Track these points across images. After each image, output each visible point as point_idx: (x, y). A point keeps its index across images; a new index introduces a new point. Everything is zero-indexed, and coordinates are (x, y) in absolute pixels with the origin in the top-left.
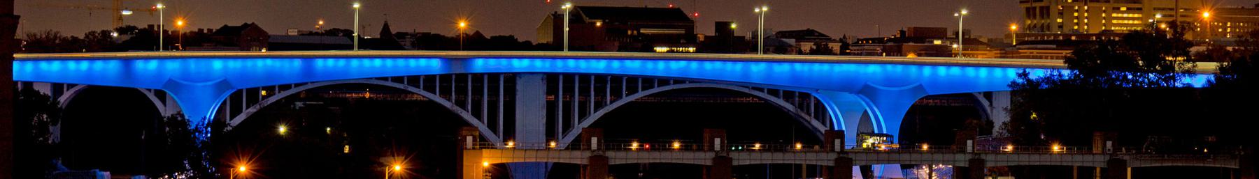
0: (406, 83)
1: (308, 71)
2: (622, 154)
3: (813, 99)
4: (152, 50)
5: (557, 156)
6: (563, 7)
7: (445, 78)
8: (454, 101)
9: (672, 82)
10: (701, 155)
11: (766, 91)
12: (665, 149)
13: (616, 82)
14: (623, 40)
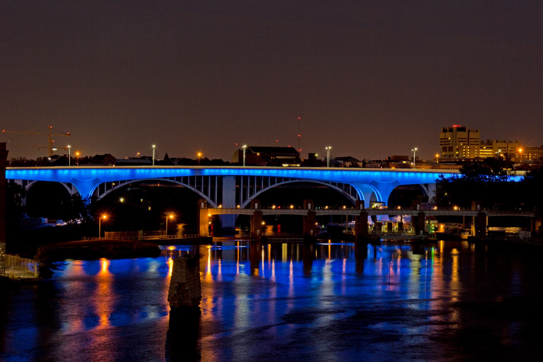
2: (268, 211)
6: (243, 147)
7: (192, 178)
9: (290, 179)
12: (287, 209)
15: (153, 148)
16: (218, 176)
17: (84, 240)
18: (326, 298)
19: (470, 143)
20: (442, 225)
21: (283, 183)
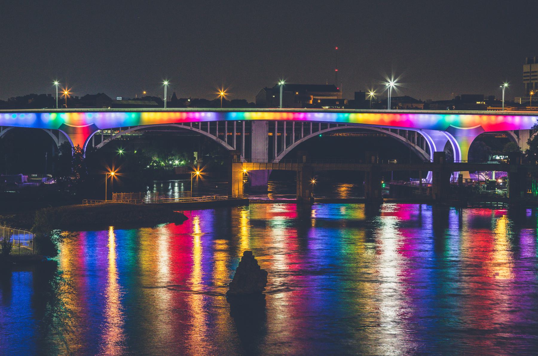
0: (191, 126)
3: (416, 134)
4: (52, 108)
8: (217, 136)
9: (338, 125)
15: (55, 87)
16: (210, 121)
17: (86, 203)
18: (283, 270)
21: (329, 130)
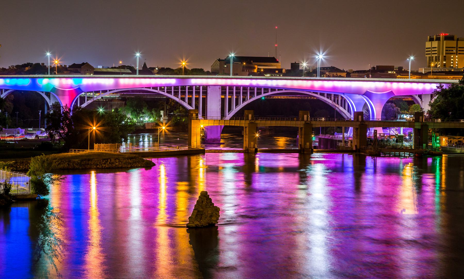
1: (117, 84)
5: (433, 125)
6: (230, 56)
7: (176, 88)
8: (180, 98)
9: (277, 90)
10: (299, 122)
11: (319, 94)
13: (252, 90)
14: (250, 71)
17: (72, 152)
19: (459, 52)
20: (444, 138)
21: (270, 93)
